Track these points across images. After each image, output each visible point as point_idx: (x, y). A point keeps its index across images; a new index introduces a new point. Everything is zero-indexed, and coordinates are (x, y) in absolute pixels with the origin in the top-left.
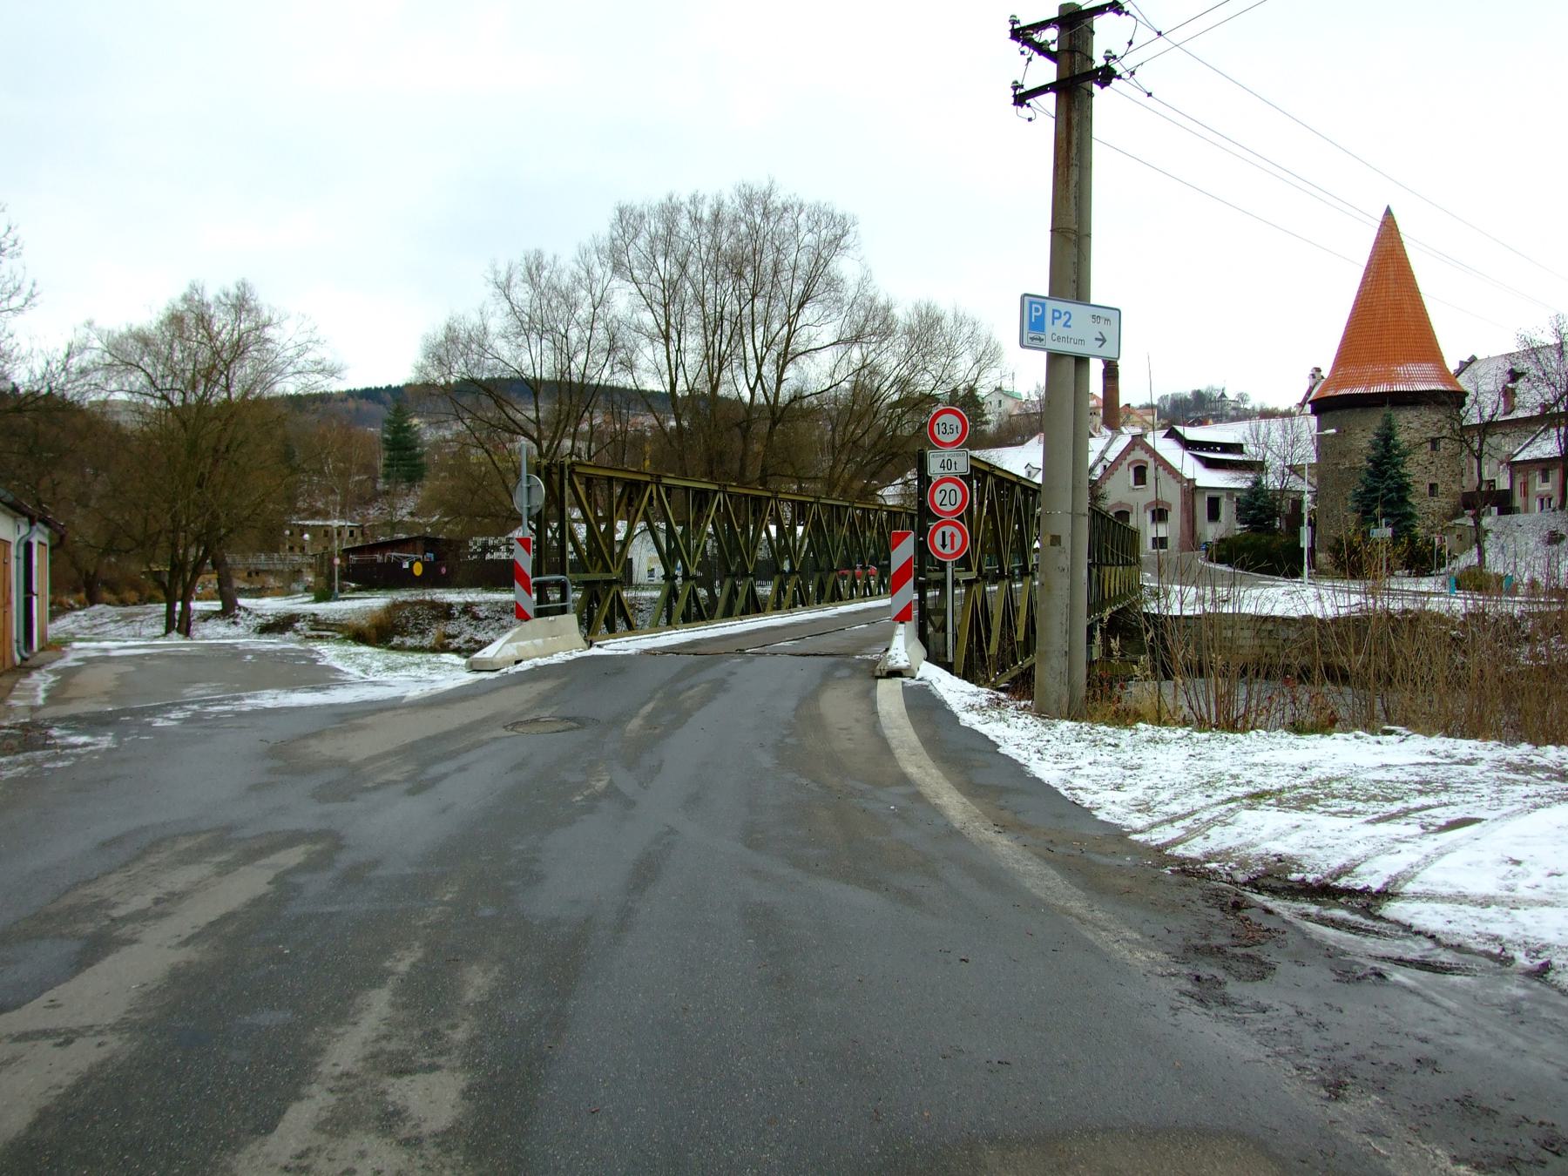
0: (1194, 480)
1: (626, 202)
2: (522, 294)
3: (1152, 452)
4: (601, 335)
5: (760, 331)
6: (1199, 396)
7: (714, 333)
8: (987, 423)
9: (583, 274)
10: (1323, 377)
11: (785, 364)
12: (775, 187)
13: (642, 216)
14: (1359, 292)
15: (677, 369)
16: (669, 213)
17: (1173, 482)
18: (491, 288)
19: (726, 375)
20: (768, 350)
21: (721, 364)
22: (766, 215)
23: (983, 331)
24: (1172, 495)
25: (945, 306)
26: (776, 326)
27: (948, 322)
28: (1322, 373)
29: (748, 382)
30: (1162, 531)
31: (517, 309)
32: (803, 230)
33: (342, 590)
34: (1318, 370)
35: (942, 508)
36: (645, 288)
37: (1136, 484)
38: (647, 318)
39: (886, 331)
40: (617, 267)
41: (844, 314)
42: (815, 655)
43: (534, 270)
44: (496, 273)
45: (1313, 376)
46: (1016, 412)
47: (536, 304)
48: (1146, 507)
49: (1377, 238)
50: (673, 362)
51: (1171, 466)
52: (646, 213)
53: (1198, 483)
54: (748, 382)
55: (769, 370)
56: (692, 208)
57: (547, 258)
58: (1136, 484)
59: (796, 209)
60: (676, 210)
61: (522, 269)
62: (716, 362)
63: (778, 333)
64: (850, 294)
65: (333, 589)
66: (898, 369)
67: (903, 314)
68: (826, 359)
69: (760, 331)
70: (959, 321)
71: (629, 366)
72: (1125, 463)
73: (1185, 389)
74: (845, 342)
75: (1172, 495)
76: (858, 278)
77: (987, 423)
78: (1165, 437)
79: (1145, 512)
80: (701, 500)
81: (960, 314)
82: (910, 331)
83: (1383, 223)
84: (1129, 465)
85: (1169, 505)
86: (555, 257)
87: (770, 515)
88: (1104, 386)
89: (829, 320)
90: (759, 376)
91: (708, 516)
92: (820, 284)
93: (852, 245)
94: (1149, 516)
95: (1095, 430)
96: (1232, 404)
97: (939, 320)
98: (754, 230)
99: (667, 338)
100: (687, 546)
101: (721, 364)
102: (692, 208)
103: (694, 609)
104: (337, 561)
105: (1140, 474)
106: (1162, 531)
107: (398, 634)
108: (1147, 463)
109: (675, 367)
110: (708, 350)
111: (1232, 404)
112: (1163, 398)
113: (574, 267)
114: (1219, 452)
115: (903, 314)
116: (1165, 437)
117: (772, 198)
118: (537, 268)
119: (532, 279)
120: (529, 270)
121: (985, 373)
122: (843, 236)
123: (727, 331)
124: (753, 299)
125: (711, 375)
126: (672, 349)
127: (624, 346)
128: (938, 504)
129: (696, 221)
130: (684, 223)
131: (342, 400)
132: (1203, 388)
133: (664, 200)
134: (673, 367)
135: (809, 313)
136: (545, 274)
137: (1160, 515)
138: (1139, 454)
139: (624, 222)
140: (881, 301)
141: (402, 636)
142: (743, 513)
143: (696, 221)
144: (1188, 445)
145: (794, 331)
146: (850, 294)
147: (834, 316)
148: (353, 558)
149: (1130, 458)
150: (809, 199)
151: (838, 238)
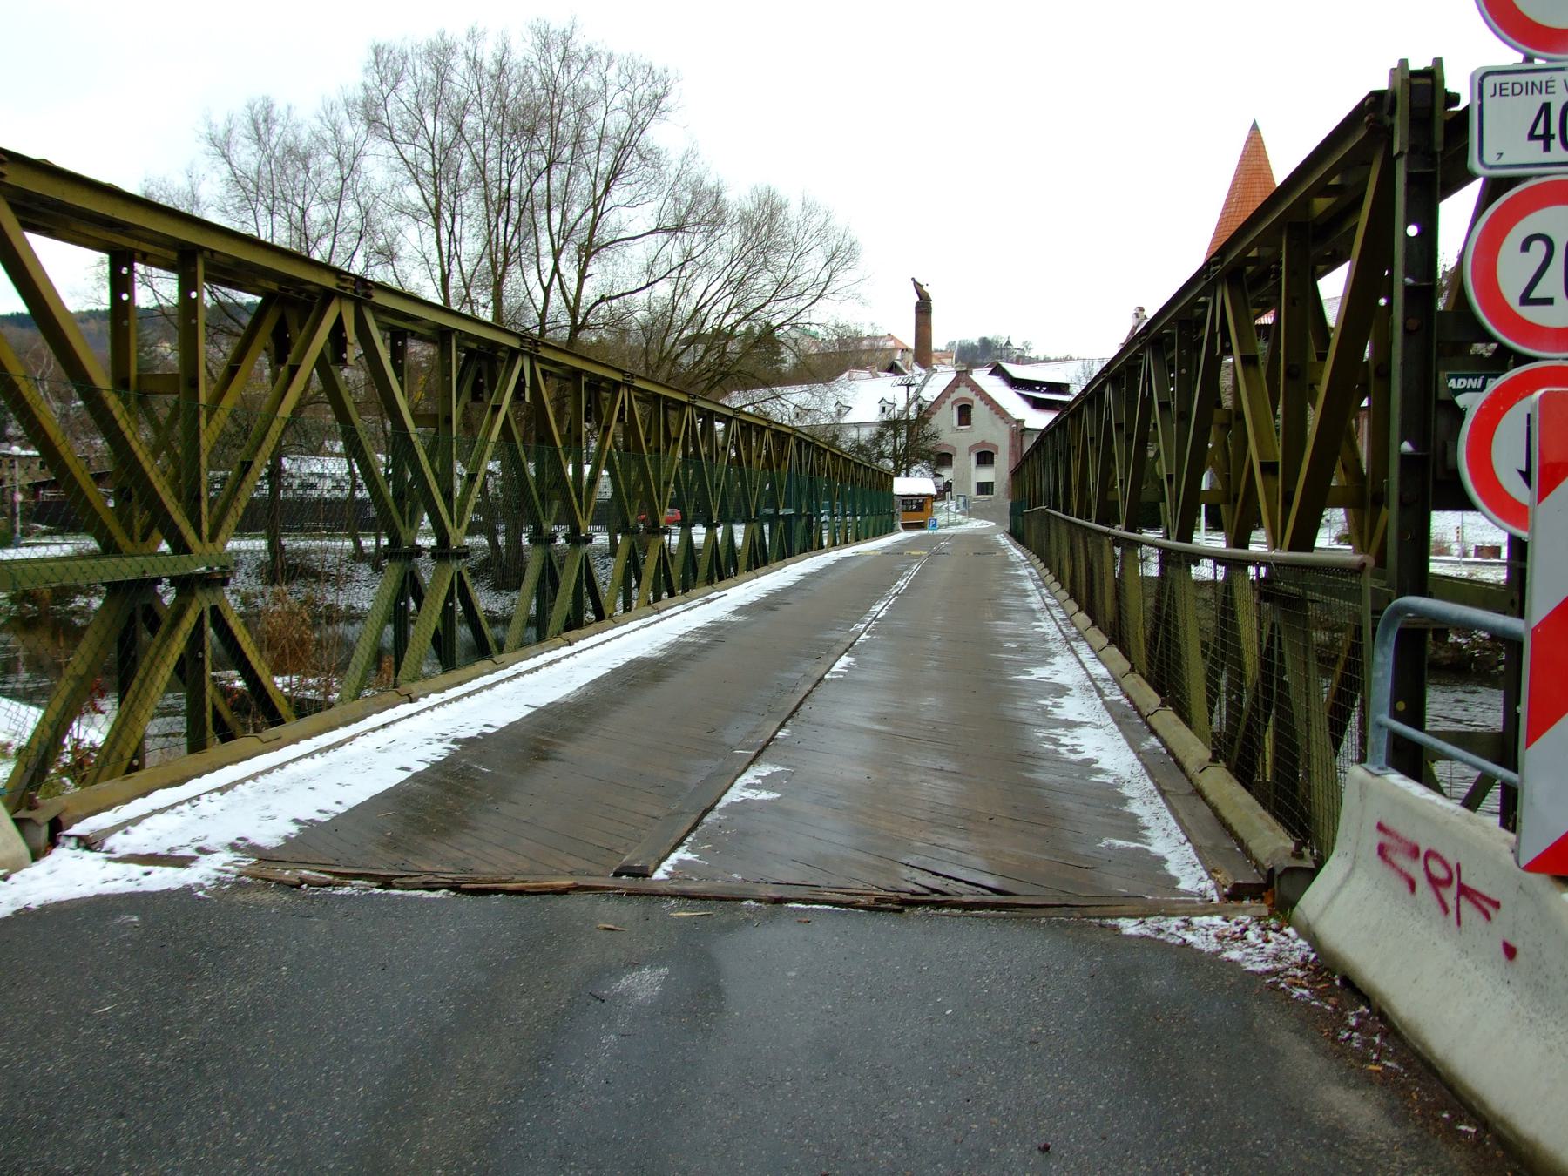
0: (1023, 421)
1: (381, 41)
2: (247, 156)
3: (975, 388)
4: (351, 211)
5: (556, 216)
6: (985, 342)
7: (498, 215)
8: (783, 361)
9: (328, 134)
10: (1146, 318)
11: (588, 257)
12: (578, 23)
13: (405, 58)
14: (1222, 214)
15: (449, 264)
16: (440, 57)
17: (1000, 423)
18: (205, 145)
19: (514, 272)
20: (566, 240)
21: (506, 259)
22: (565, 60)
23: (838, 222)
24: (1000, 439)
25: (791, 196)
26: (577, 210)
27: (794, 211)
28: (1145, 313)
29: (540, 279)
30: (986, 475)
31: (238, 172)
32: (612, 90)
33: (27, 533)
34: (1142, 309)
35: (1531, 314)
36: (409, 153)
37: (960, 424)
38: (413, 195)
39: (716, 219)
40: (373, 123)
41: (665, 194)
42: (924, 870)
43: (262, 124)
44: (211, 126)
45: (1137, 315)
46: (814, 350)
47: (265, 170)
48: (971, 449)
49: (1243, 155)
50: (445, 250)
51: (998, 406)
52: (409, 52)
53: (1027, 425)
54: (540, 279)
55: (569, 271)
56: (469, 45)
57: (279, 109)
58: (960, 424)
59: (604, 59)
60: (448, 50)
61: (246, 120)
62: (500, 261)
63: (577, 221)
64: (671, 172)
65: (14, 531)
66: (729, 269)
67: (738, 196)
68: (639, 253)
69: (556, 216)
70: (809, 209)
71: (388, 255)
72: (949, 402)
73: (974, 339)
74: (667, 230)
75: (1000, 439)
76: (681, 153)
77: (783, 361)
78: (990, 374)
79: (970, 455)
80: (479, 374)
81: (810, 200)
82: (745, 218)
83: (1250, 139)
84: (953, 403)
85: (996, 448)
86: (289, 108)
87: (620, 420)
88: (917, 322)
89: (647, 198)
90: (556, 270)
91: (496, 409)
92: (633, 161)
93: (674, 108)
94: (973, 459)
95: (907, 367)
96: (1018, 352)
97: (782, 207)
98: (551, 87)
99: (437, 216)
100: (445, 478)
101: (506, 259)
102: (469, 45)
103: (463, 633)
104: (19, 497)
105: (965, 413)
106: (986, 475)
107: (81, 593)
108: (972, 401)
109: (447, 260)
110: (490, 234)
111: (1018, 352)
112: (951, 344)
113: (317, 125)
114: (1045, 392)
115: (738, 196)
116: (990, 374)
117: (574, 39)
118: (265, 121)
119: (260, 138)
120: (255, 123)
121: (840, 274)
122: (665, 94)
123: (515, 215)
124: (549, 168)
125: (494, 268)
126: (445, 236)
127: (375, 197)
128: (1511, 294)
129: (475, 66)
130: (460, 65)
131: (82, 321)
132: (990, 337)
133: (435, 38)
134: (445, 259)
135: (618, 194)
136: (277, 129)
137: (985, 458)
138: (964, 392)
139: (381, 68)
140: (709, 182)
141: (87, 595)
142: (569, 409)
143: (475, 66)
144: (1015, 383)
145: (602, 213)
146: (671, 172)
147: (653, 195)
148: (46, 494)
149: (954, 396)
150: (620, 51)
151: (658, 98)
